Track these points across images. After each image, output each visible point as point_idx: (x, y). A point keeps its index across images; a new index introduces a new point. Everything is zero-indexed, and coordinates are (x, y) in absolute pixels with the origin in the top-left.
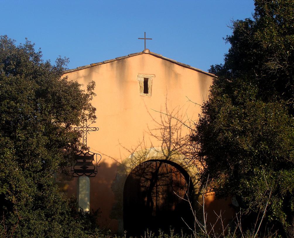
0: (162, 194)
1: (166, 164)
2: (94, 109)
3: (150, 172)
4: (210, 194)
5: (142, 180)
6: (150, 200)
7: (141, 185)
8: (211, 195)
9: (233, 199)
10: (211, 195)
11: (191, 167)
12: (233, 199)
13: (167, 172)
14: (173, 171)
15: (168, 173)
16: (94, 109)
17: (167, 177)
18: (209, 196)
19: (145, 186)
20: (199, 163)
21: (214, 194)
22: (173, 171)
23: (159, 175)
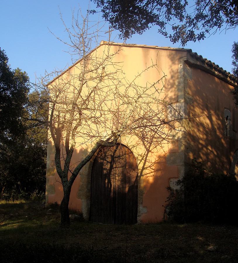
0: (118, 176)
1: (50, 128)
2: (174, 34)
3: (110, 155)
4: (150, 176)
5: (105, 163)
6: (109, 182)
7: (104, 167)
8: (151, 176)
9: (171, 181)
10: (151, 176)
11: (134, 148)
12: (171, 181)
13: (123, 154)
14: (127, 153)
15: (123, 155)
16: (174, 34)
17: (122, 159)
18: (149, 177)
19: (106, 169)
20: (141, 143)
21: (153, 175)
22: (127, 153)
23: (116, 158)
